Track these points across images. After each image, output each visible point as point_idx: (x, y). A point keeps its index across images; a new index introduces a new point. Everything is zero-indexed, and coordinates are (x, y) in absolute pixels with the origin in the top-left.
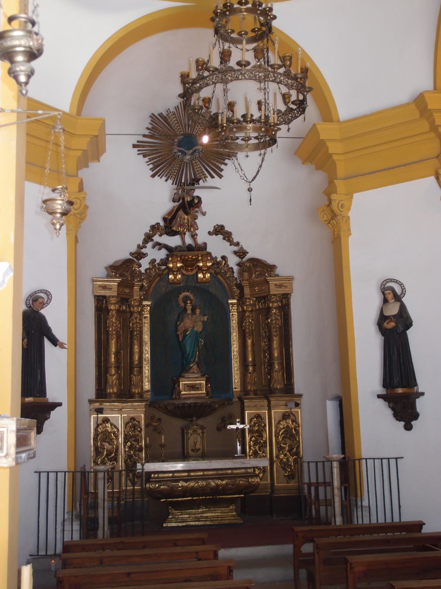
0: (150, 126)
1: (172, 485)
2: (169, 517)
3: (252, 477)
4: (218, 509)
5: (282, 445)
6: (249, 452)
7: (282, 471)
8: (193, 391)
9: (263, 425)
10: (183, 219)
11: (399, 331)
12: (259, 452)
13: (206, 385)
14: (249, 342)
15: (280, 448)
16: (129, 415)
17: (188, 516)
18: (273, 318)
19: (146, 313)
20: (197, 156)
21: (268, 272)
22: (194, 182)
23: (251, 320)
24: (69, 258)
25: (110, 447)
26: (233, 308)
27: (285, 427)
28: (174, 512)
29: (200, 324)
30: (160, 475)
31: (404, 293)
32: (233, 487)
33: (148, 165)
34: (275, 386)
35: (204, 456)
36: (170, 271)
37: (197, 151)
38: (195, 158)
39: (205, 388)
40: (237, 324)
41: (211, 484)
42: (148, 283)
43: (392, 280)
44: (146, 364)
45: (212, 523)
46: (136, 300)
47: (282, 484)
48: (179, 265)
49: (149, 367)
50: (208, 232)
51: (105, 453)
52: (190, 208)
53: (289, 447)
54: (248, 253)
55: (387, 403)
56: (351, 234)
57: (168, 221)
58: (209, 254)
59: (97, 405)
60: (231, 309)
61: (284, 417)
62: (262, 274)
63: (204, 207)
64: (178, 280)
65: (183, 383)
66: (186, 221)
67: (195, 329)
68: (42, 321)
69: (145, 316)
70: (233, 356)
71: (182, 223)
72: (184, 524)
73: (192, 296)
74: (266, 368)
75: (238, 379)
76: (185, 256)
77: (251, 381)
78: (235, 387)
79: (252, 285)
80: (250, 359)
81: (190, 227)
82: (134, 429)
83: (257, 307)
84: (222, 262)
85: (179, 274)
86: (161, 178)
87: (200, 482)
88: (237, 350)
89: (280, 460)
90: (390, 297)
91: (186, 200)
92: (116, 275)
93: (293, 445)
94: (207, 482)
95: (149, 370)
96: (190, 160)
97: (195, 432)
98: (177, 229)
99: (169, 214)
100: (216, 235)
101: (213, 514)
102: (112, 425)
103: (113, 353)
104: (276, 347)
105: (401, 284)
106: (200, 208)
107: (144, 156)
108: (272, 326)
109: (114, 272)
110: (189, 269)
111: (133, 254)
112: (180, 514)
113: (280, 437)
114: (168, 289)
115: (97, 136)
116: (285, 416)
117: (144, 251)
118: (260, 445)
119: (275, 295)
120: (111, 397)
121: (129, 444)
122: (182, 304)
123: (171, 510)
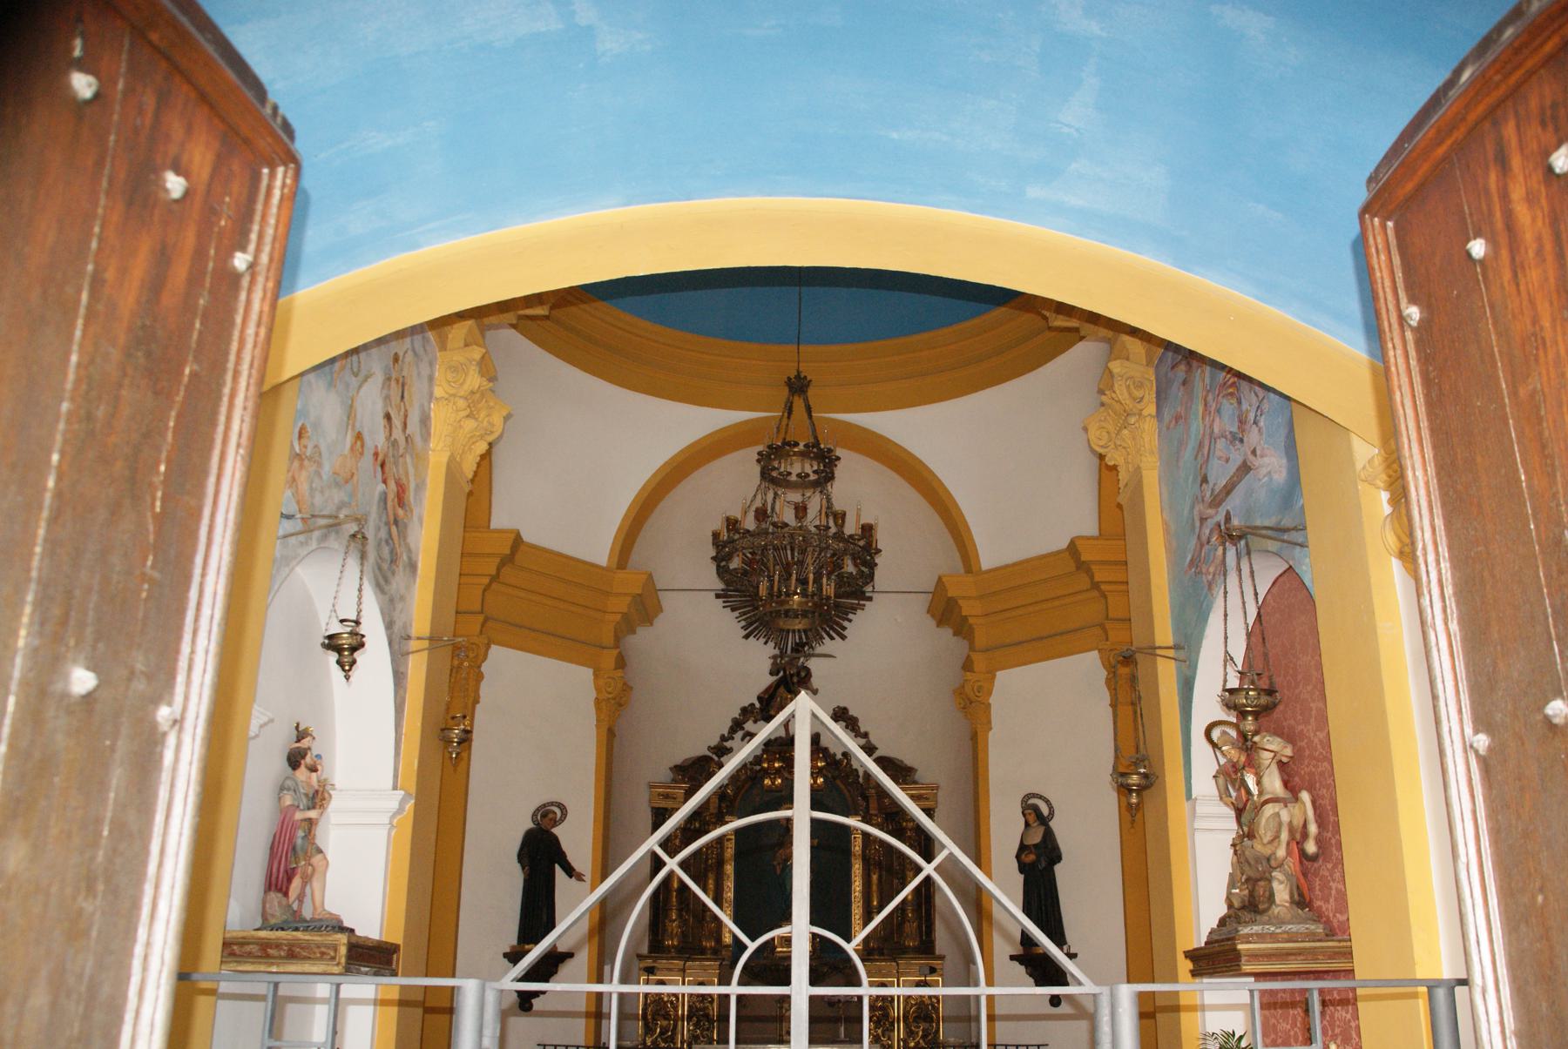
5: (913, 1028)
14: (875, 877)
24: (598, 757)
36: (766, 773)
46: (712, 814)
51: (658, 1030)
54: (877, 749)
56: (991, 729)
59: (649, 963)
64: (777, 786)
68: (555, 842)
80: (875, 903)
84: (843, 761)
90: (1032, 818)
92: (683, 779)
107: (733, 610)
111: (712, 748)
115: (639, 595)
117: (728, 744)
120: (670, 952)
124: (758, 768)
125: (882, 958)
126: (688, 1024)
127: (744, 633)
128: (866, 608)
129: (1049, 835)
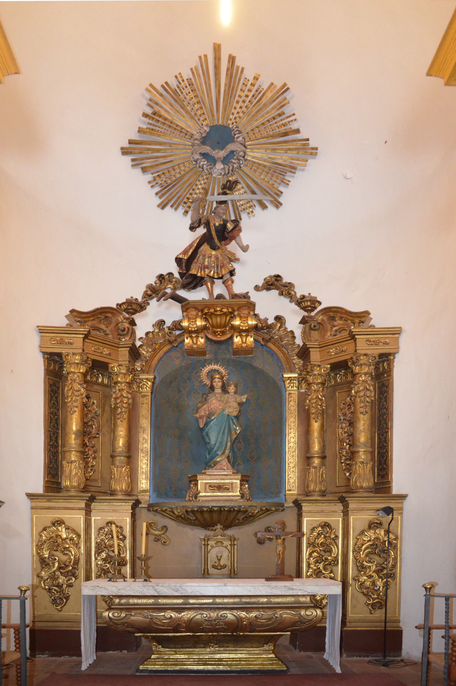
0: (149, 111)
1: (150, 615)
2: (152, 657)
3: (307, 608)
7: (363, 599)
8: (219, 492)
12: (323, 572)
13: (241, 485)
14: (316, 425)
15: (361, 568)
16: (104, 518)
19: (145, 390)
21: (354, 325)
22: (225, 190)
23: (321, 395)
25: (64, 558)
26: (292, 385)
27: (373, 539)
29: (236, 405)
30: (131, 601)
32: (270, 622)
37: (235, 157)
38: (232, 170)
39: (239, 489)
40: (296, 407)
44: (143, 456)
45: (229, 669)
49: (147, 461)
50: (254, 287)
51: (56, 565)
53: (376, 567)
57: (184, 264)
61: (372, 526)
65: (202, 481)
66: (213, 260)
67: (226, 412)
69: (142, 394)
70: (289, 448)
71: (206, 263)
72: (178, 668)
73: (222, 370)
74: (342, 463)
75: (294, 478)
78: (289, 489)
81: (219, 269)
85: (202, 338)
86: (176, 209)
87: (205, 613)
88: (295, 441)
89: (359, 584)
93: (384, 563)
94: (220, 614)
95: (147, 465)
97: (219, 544)
99: (185, 252)
100: (268, 289)
102: (67, 528)
103: (72, 432)
104: (364, 429)
106: (237, 238)
107: (144, 170)
109: (79, 321)
110: (218, 331)
112: (172, 653)
113: (361, 553)
114: (185, 362)
116: (373, 525)
118: (327, 563)
119: (366, 355)
121: (104, 555)
126: (96, 559)
127: (159, 201)
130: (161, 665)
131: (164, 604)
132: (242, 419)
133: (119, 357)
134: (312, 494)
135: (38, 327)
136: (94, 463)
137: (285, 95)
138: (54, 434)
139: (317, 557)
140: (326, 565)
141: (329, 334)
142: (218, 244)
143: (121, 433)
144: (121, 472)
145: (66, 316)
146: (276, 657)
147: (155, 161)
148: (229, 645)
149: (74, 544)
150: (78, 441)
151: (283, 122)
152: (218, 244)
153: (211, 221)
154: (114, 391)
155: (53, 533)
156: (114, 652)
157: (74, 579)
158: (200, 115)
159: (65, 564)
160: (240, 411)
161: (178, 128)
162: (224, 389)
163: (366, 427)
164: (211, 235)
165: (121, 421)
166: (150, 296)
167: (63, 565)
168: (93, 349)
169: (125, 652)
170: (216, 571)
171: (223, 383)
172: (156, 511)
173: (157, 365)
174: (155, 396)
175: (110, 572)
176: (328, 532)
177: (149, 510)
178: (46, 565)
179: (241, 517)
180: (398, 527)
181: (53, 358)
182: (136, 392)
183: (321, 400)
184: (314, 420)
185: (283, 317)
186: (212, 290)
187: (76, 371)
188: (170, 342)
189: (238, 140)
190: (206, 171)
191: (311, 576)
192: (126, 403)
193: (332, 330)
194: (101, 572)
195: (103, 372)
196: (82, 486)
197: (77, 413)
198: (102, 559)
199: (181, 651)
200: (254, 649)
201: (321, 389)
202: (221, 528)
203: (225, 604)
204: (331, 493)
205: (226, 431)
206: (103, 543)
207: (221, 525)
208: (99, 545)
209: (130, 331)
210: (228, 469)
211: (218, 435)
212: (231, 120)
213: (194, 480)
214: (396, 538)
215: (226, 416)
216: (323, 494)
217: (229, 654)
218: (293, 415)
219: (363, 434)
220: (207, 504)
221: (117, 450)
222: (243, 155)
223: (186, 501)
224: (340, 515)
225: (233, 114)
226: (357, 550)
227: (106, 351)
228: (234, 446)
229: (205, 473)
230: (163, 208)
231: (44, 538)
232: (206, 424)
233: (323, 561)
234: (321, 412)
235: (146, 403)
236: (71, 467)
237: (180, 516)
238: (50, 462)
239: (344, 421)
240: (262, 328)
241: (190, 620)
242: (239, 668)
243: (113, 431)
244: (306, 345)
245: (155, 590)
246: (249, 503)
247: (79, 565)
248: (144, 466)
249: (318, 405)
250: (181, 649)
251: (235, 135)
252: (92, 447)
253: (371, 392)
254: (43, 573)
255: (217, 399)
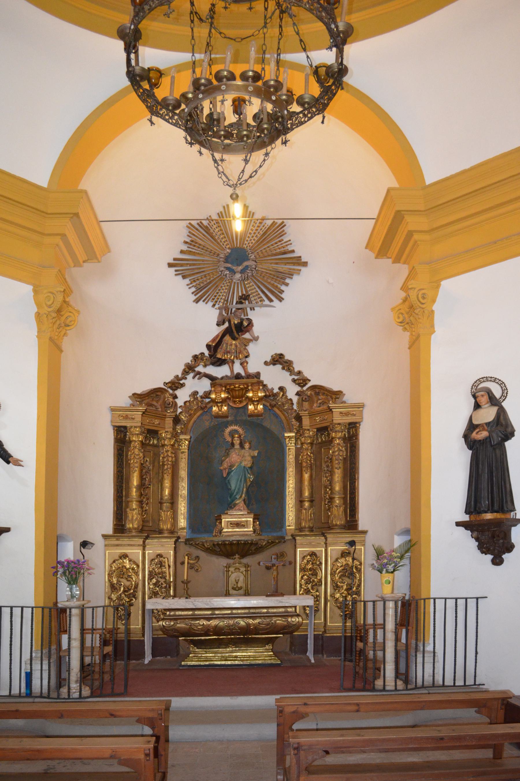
0: (188, 240)
1: (190, 623)
3: (292, 616)
4: (251, 648)
5: (339, 584)
6: (300, 591)
9: (318, 563)
10: (230, 345)
11: (494, 443)
12: (312, 591)
13: (254, 522)
14: (306, 476)
16: (155, 552)
17: (213, 655)
18: (336, 449)
20: (250, 274)
22: (241, 300)
23: (310, 453)
25: (128, 583)
26: (291, 442)
28: (197, 650)
29: (249, 458)
30: (178, 613)
31: (505, 395)
32: (268, 627)
33: (190, 288)
34: (334, 523)
35: (247, 594)
36: (214, 402)
37: (249, 269)
38: (247, 277)
39: (252, 526)
41: (240, 623)
42: (187, 417)
43: (487, 379)
45: (242, 663)
46: (167, 432)
47: (336, 623)
48: (223, 395)
51: (122, 589)
52: (238, 333)
55: (469, 532)
57: (212, 349)
58: (262, 382)
60: (287, 442)
61: (343, 555)
62: (326, 403)
63: (256, 330)
65: (225, 520)
66: (233, 347)
67: (243, 464)
69: (182, 451)
70: (288, 493)
71: (228, 349)
72: (207, 663)
73: (240, 430)
74: (326, 504)
76: (230, 385)
77: (306, 517)
79: (311, 415)
81: (238, 354)
82: (161, 567)
83: (320, 440)
85: (225, 406)
86: (206, 303)
90: (484, 400)
91: (232, 323)
94: (235, 621)
95: (185, 507)
96: (241, 279)
97: (237, 570)
98: (222, 357)
99: (213, 340)
100: (274, 364)
101: (245, 654)
102: (130, 561)
103: (134, 487)
105: (501, 384)
106: (251, 332)
107: (184, 277)
108: (334, 458)
109: (138, 401)
111: (167, 384)
112: (204, 652)
113: (336, 576)
114: (213, 423)
116: (344, 554)
118: (314, 584)
119: (339, 424)
121: (154, 580)
122: (229, 439)
123: (193, 649)
124: (208, 400)
125: (312, 533)
126: (149, 584)
128: (301, 273)
129: (502, 413)
130: (196, 661)
131: (199, 615)
132: (255, 468)
133: (166, 425)
134: (304, 529)
135: (110, 407)
136: (147, 508)
137: (283, 229)
138: (120, 488)
139: (307, 579)
140: (313, 585)
141: (315, 405)
142: (237, 336)
143: (167, 485)
144: (167, 515)
145: (129, 397)
146: (274, 654)
147: (192, 271)
148: (242, 646)
149: (134, 573)
150: (138, 493)
151: (283, 245)
152: (237, 336)
153: (231, 320)
154: (162, 451)
155: (120, 564)
156: (161, 658)
157: (134, 599)
158: (224, 242)
159: (128, 588)
160: (253, 463)
161: (208, 250)
162: (242, 446)
163: (340, 479)
164: (232, 330)
165: (167, 476)
166: (187, 373)
167: (127, 589)
168: (148, 421)
169: (169, 657)
170: (235, 592)
171: (241, 440)
172: (191, 544)
173: (192, 427)
174: (191, 452)
175: (159, 594)
176: (314, 559)
177: (186, 544)
178: (114, 589)
179: (253, 548)
180: (362, 555)
181: (120, 429)
182: (177, 449)
183: (310, 456)
184: (305, 472)
185: (285, 388)
186: (233, 369)
187: (137, 440)
188: (202, 408)
189: (251, 257)
190: (228, 278)
191: (303, 594)
192: (171, 461)
193: (317, 402)
194: (152, 594)
195: (153, 436)
196: (141, 527)
197: (137, 472)
198: (153, 584)
199: (210, 651)
200: (259, 648)
201: (310, 448)
202: (238, 558)
203: (239, 614)
204: (319, 528)
205: (243, 479)
206: (154, 571)
207: (238, 555)
208: (151, 573)
209: (174, 405)
210: (244, 509)
211: (237, 483)
212: (246, 244)
213: (219, 519)
214: (361, 564)
215: (243, 468)
216: (311, 529)
217: (243, 652)
218: (291, 465)
219: (337, 484)
220: (228, 539)
221: (164, 498)
222: (255, 267)
223: (214, 536)
224: (323, 546)
225: (247, 241)
226: (333, 574)
227: (157, 422)
228: (250, 489)
229: (227, 513)
230: (197, 303)
231: (114, 568)
232: (229, 474)
233: (311, 582)
234: (310, 466)
235: (184, 458)
236: (133, 513)
237: (209, 548)
238: (117, 509)
239: (328, 472)
240: (270, 396)
241: (216, 626)
242: (248, 663)
243: (161, 482)
244: (299, 414)
245: (194, 605)
246: (259, 537)
247: (138, 589)
248: (183, 509)
249: (308, 460)
250: (210, 650)
251: (249, 254)
252: (146, 496)
253: (343, 452)
254: (113, 595)
255: (236, 453)
